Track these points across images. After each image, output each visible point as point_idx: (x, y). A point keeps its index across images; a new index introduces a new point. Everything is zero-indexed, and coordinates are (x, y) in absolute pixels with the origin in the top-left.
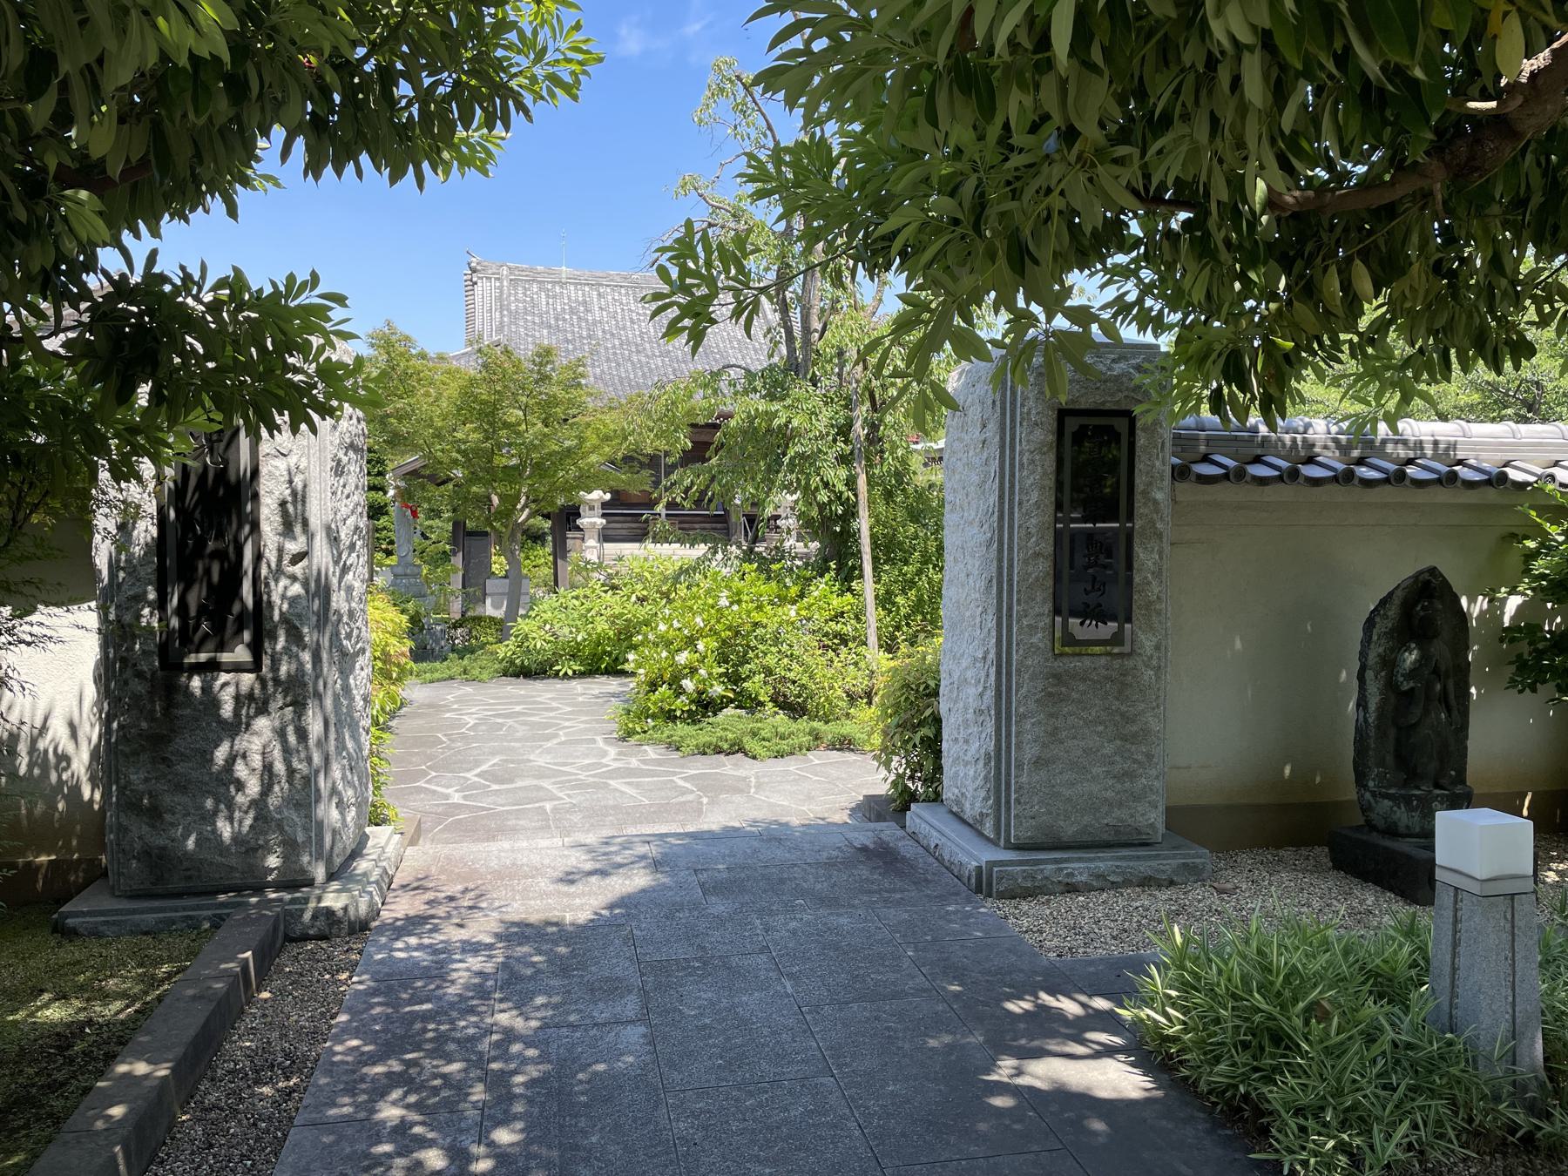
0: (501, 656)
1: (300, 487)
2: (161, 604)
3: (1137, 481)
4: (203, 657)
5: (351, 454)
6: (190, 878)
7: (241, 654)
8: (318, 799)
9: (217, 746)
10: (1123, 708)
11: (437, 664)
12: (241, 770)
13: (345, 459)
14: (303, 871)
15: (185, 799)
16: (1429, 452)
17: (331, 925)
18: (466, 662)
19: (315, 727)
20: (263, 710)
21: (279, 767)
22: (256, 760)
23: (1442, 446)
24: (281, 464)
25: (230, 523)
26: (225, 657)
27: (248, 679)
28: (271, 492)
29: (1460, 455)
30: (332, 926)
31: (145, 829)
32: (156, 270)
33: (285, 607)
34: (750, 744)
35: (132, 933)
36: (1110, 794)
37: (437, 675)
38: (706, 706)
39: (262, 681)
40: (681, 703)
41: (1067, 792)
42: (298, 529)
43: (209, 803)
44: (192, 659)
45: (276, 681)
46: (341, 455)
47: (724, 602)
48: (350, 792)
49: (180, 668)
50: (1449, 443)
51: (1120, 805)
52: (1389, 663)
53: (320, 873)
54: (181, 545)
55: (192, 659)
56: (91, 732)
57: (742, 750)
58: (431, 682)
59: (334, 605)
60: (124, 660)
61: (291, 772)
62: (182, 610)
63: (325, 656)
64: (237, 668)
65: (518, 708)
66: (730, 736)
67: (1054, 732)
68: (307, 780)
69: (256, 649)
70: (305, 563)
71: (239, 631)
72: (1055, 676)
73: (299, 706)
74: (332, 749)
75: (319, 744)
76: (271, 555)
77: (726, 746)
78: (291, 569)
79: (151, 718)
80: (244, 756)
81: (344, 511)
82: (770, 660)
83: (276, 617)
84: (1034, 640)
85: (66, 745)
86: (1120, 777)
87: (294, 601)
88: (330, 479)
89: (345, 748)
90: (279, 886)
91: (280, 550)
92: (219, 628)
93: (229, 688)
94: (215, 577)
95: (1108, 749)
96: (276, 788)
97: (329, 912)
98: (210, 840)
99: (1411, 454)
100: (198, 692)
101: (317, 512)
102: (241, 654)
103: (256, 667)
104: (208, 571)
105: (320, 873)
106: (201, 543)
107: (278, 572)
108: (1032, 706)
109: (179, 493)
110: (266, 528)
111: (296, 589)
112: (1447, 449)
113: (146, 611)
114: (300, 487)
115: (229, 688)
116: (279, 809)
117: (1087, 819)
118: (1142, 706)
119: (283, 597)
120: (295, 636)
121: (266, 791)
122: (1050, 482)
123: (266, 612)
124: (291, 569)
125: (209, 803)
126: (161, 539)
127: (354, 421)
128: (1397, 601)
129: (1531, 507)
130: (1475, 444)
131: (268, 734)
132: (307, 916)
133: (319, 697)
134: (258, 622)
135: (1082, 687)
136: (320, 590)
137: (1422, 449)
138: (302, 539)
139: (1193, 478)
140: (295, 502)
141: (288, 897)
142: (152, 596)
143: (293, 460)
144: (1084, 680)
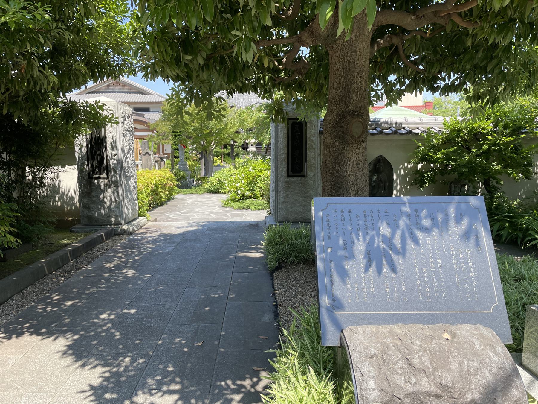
0: (206, 187)
1: (115, 140)
2: (88, 165)
3: (308, 135)
4: (97, 176)
5: (127, 132)
6: (96, 222)
7: (104, 175)
8: (122, 207)
9: (100, 195)
10: (305, 190)
11: (189, 190)
12: (106, 200)
13: (125, 133)
14: (119, 222)
15: (94, 205)
16: (394, 126)
17: (124, 232)
18: (197, 189)
19: (121, 192)
20: (109, 187)
21: (113, 199)
22: (109, 198)
23: (398, 124)
24: (111, 135)
25: (101, 147)
26: (101, 176)
27: (106, 180)
28: (109, 141)
29: (403, 126)
30: (125, 233)
31: (87, 212)
32: (71, 101)
33: (113, 166)
34: (251, 207)
35: (85, 232)
36: (301, 210)
37: (188, 192)
38: (244, 197)
39: (109, 181)
40: (238, 197)
41: (291, 210)
42: (115, 149)
43: (100, 207)
44: (95, 176)
45: (112, 181)
46: (124, 132)
47: (250, 169)
48: (130, 206)
49: (92, 178)
50: (400, 123)
51: (304, 213)
52: (370, 179)
53: (123, 222)
54: (91, 153)
55: (95, 176)
56: (78, 193)
57: (250, 208)
58: (186, 194)
59: (124, 165)
60: (81, 176)
61: (116, 200)
62: (92, 166)
63: (122, 176)
64: (104, 178)
65: (203, 200)
66: (247, 204)
67: (287, 195)
68: (119, 202)
69: (107, 174)
70: (117, 156)
71: (104, 171)
72: (287, 182)
73: (117, 186)
74: (125, 195)
75: (122, 195)
76: (110, 155)
77: (245, 207)
78: (114, 157)
79: (87, 188)
80: (106, 197)
81: (126, 145)
82: (261, 185)
83: (111, 168)
84: (282, 174)
85: (74, 195)
86: (304, 206)
87: (115, 164)
88: (121, 138)
89: (128, 196)
90: (114, 224)
91: (112, 154)
92: (100, 170)
93: (102, 183)
94: (99, 159)
95: (301, 200)
96: (113, 204)
97: (124, 230)
98: (100, 214)
99: (389, 126)
100: (96, 183)
101: (119, 145)
102: (104, 175)
103: (108, 178)
104: (97, 158)
105: (123, 222)
106: (95, 152)
107: (112, 158)
108: (282, 189)
109: (91, 141)
110: (108, 148)
111: (115, 162)
112: (399, 125)
113: (85, 166)
114: (115, 140)
115: (102, 183)
116: (113, 208)
117: (296, 216)
118: (309, 189)
119: (113, 163)
120: (115, 172)
121: (111, 204)
122: (286, 136)
123: (109, 167)
124: (114, 157)
125: (100, 207)
126: (87, 151)
127: (128, 125)
128: (372, 164)
129: (416, 139)
130: (409, 123)
131: (111, 192)
132: (119, 230)
133: (121, 185)
134: (107, 169)
135: (294, 185)
136: (120, 162)
137: (392, 125)
138: (116, 151)
139: (384, 134)
140: (114, 143)
141: (115, 226)
142: (86, 163)
143: (113, 134)
144: (294, 183)
